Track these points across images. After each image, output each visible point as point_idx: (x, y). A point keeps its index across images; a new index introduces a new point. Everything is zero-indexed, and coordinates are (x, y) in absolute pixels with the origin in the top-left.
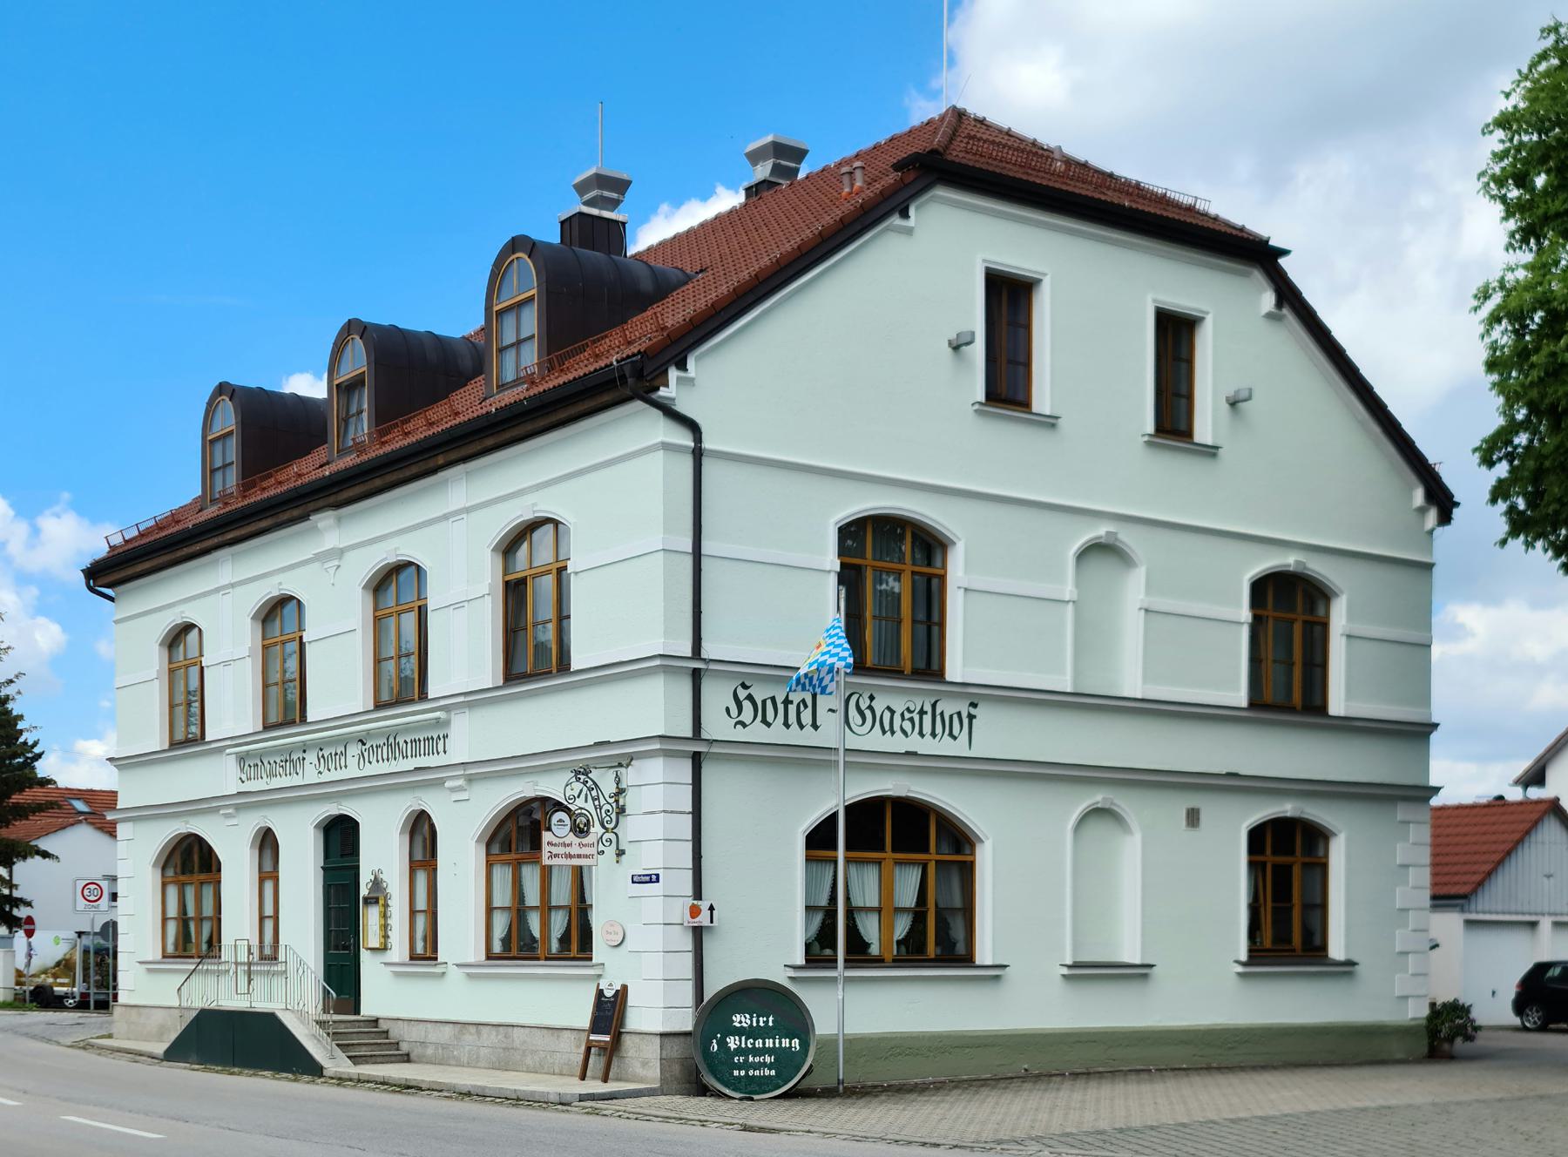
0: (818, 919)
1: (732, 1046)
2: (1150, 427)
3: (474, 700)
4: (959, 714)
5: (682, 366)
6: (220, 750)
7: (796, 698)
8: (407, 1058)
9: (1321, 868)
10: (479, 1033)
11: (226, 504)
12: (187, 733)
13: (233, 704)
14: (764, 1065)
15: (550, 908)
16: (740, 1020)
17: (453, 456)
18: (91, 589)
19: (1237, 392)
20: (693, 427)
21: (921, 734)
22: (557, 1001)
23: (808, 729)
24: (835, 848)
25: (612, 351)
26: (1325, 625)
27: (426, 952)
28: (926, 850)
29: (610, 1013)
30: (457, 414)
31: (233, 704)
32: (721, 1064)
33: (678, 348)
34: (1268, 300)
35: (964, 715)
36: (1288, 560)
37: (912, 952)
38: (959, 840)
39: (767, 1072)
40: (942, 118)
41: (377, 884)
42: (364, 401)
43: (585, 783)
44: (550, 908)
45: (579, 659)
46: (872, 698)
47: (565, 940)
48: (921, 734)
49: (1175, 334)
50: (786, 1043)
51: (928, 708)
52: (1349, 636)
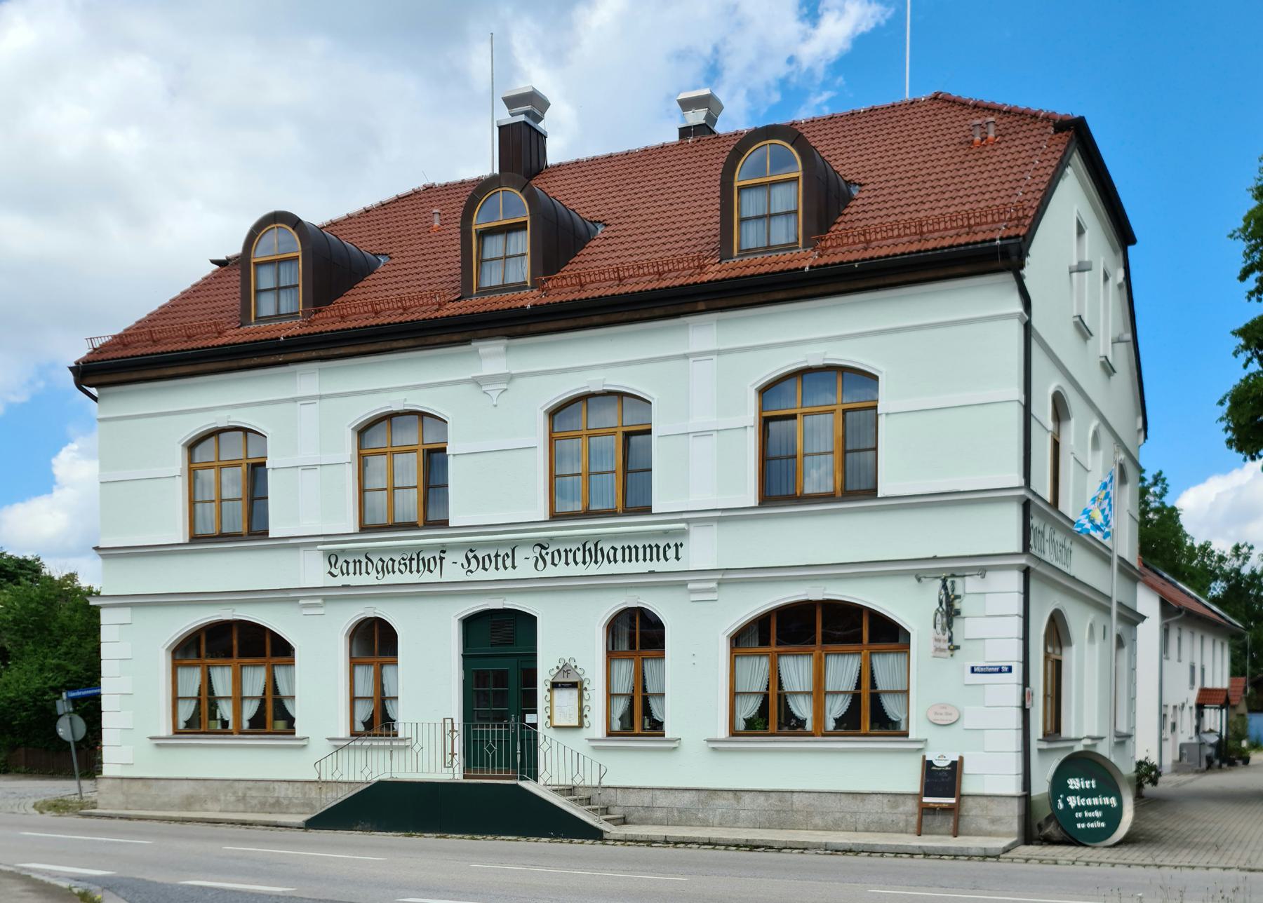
1: (1072, 804)
7: (502, 553)
14: (1093, 819)
15: (243, 698)
21: (411, 572)
22: (887, 771)
23: (510, 569)
29: (942, 780)
48: (411, 572)
50: (1106, 801)
51: (415, 556)
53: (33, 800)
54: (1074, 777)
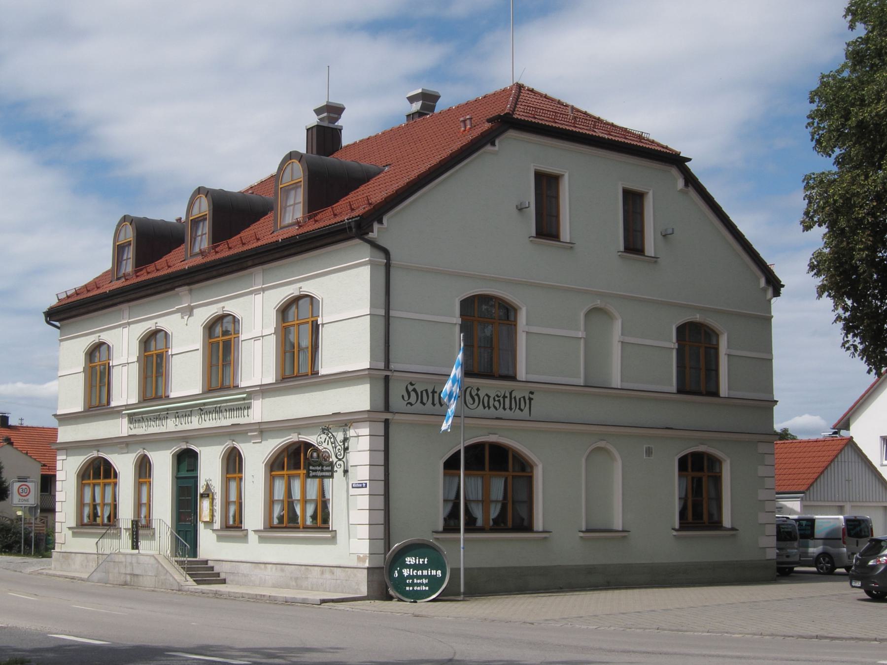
0: (450, 506)
2: (622, 248)
3: (264, 391)
4: (524, 397)
5: (380, 222)
6: (119, 412)
8: (224, 582)
9: (717, 480)
10: (266, 568)
11: (126, 280)
12: (98, 404)
13: (125, 388)
14: (422, 584)
16: (410, 560)
17: (256, 261)
18: (48, 323)
19: (666, 230)
20: (386, 253)
21: (504, 409)
24: (459, 469)
25: (344, 211)
26: (716, 349)
27: (233, 526)
28: (506, 470)
30: (258, 240)
31: (125, 388)
32: (400, 584)
33: (378, 212)
34: (680, 183)
35: (527, 398)
36: (697, 317)
37: (499, 525)
38: (524, 467)
39: (424, 588)
40: (511, 88)
41: (208, 486)
42: (205, 229)
43: (327, 435)
44: (482, 501)
45: (326, 368)
46: (478, 390)
47: (314, 517)
48: (504, 409)
49: (633, 201)
50: (434, 573)
51: (508, 395)
52: (729, 355)
53: (52, 566)
54: (411, 556)
